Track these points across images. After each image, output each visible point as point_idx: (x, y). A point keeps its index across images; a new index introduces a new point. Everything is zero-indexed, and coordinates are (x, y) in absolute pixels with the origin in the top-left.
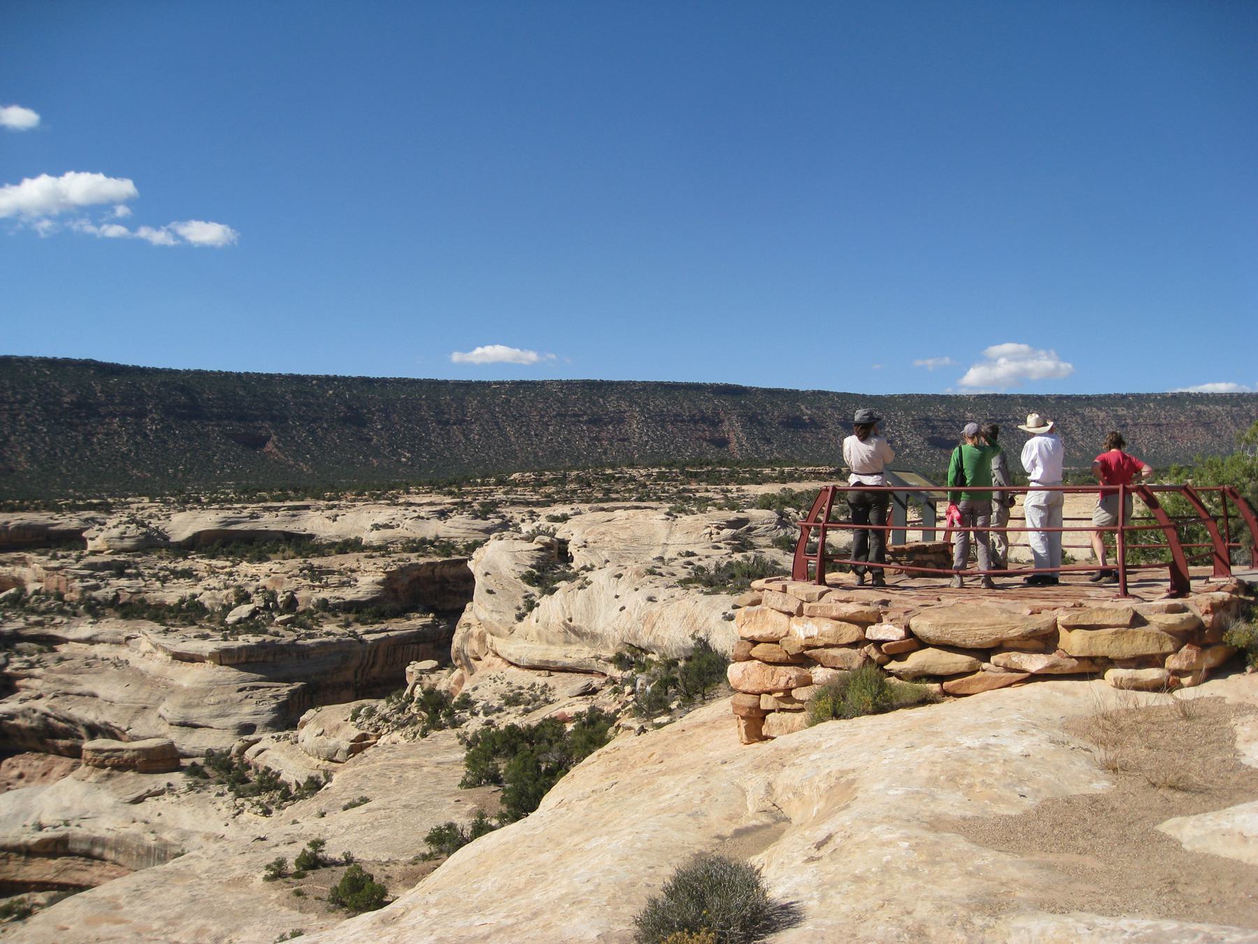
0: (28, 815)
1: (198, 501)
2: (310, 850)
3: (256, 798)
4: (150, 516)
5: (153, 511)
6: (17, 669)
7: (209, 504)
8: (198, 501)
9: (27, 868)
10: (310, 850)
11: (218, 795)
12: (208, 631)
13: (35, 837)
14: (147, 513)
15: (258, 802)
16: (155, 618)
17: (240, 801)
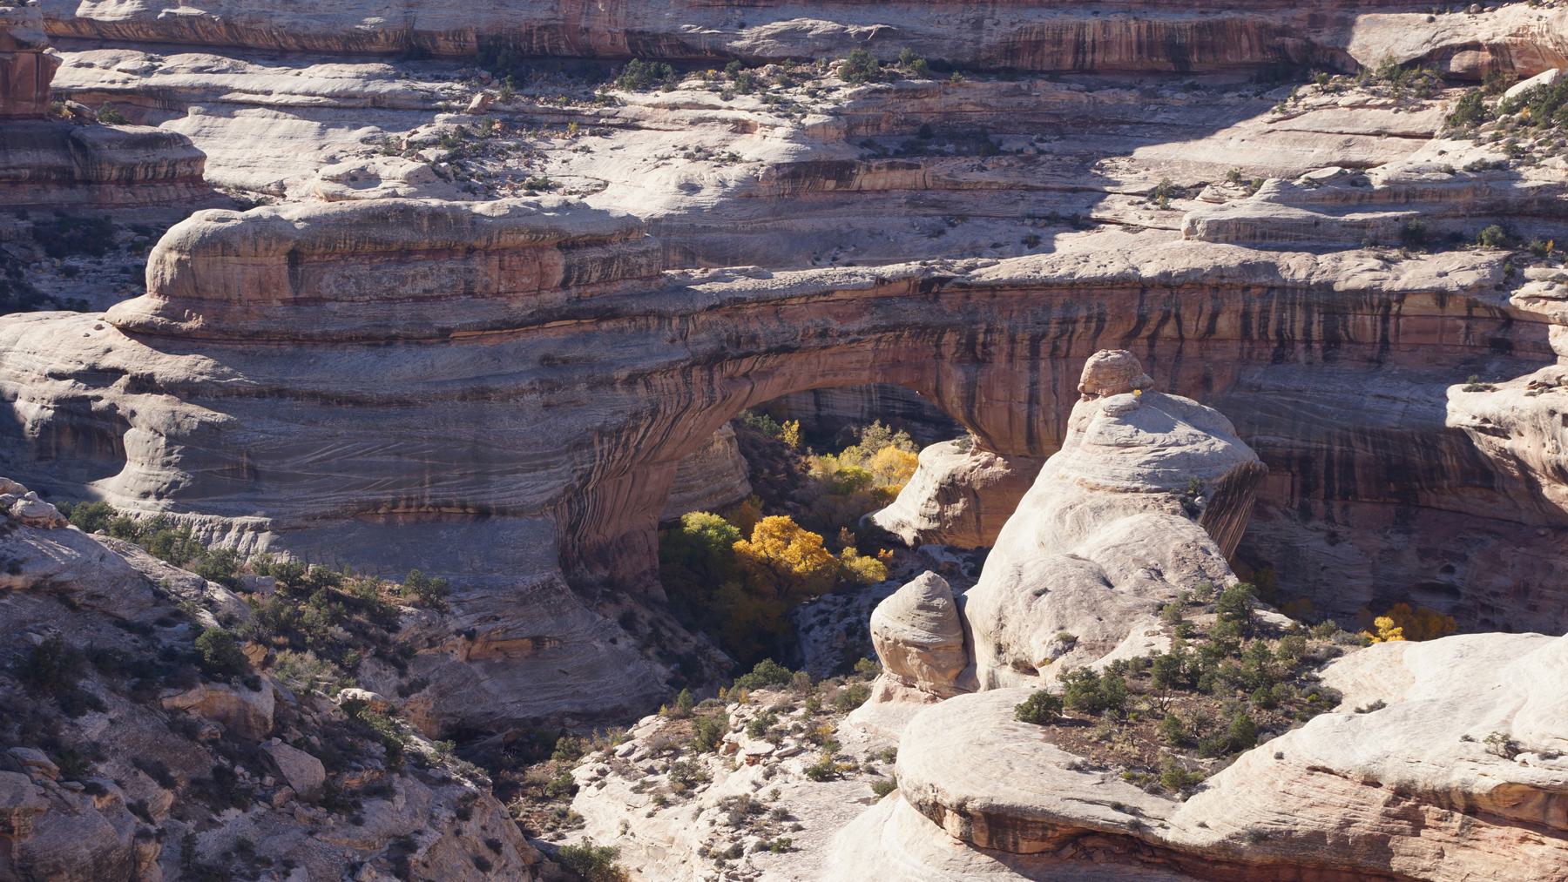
0: (1482, 711)
6: (1532, 298)
9: (1463, 855)
13: (1491, 775)
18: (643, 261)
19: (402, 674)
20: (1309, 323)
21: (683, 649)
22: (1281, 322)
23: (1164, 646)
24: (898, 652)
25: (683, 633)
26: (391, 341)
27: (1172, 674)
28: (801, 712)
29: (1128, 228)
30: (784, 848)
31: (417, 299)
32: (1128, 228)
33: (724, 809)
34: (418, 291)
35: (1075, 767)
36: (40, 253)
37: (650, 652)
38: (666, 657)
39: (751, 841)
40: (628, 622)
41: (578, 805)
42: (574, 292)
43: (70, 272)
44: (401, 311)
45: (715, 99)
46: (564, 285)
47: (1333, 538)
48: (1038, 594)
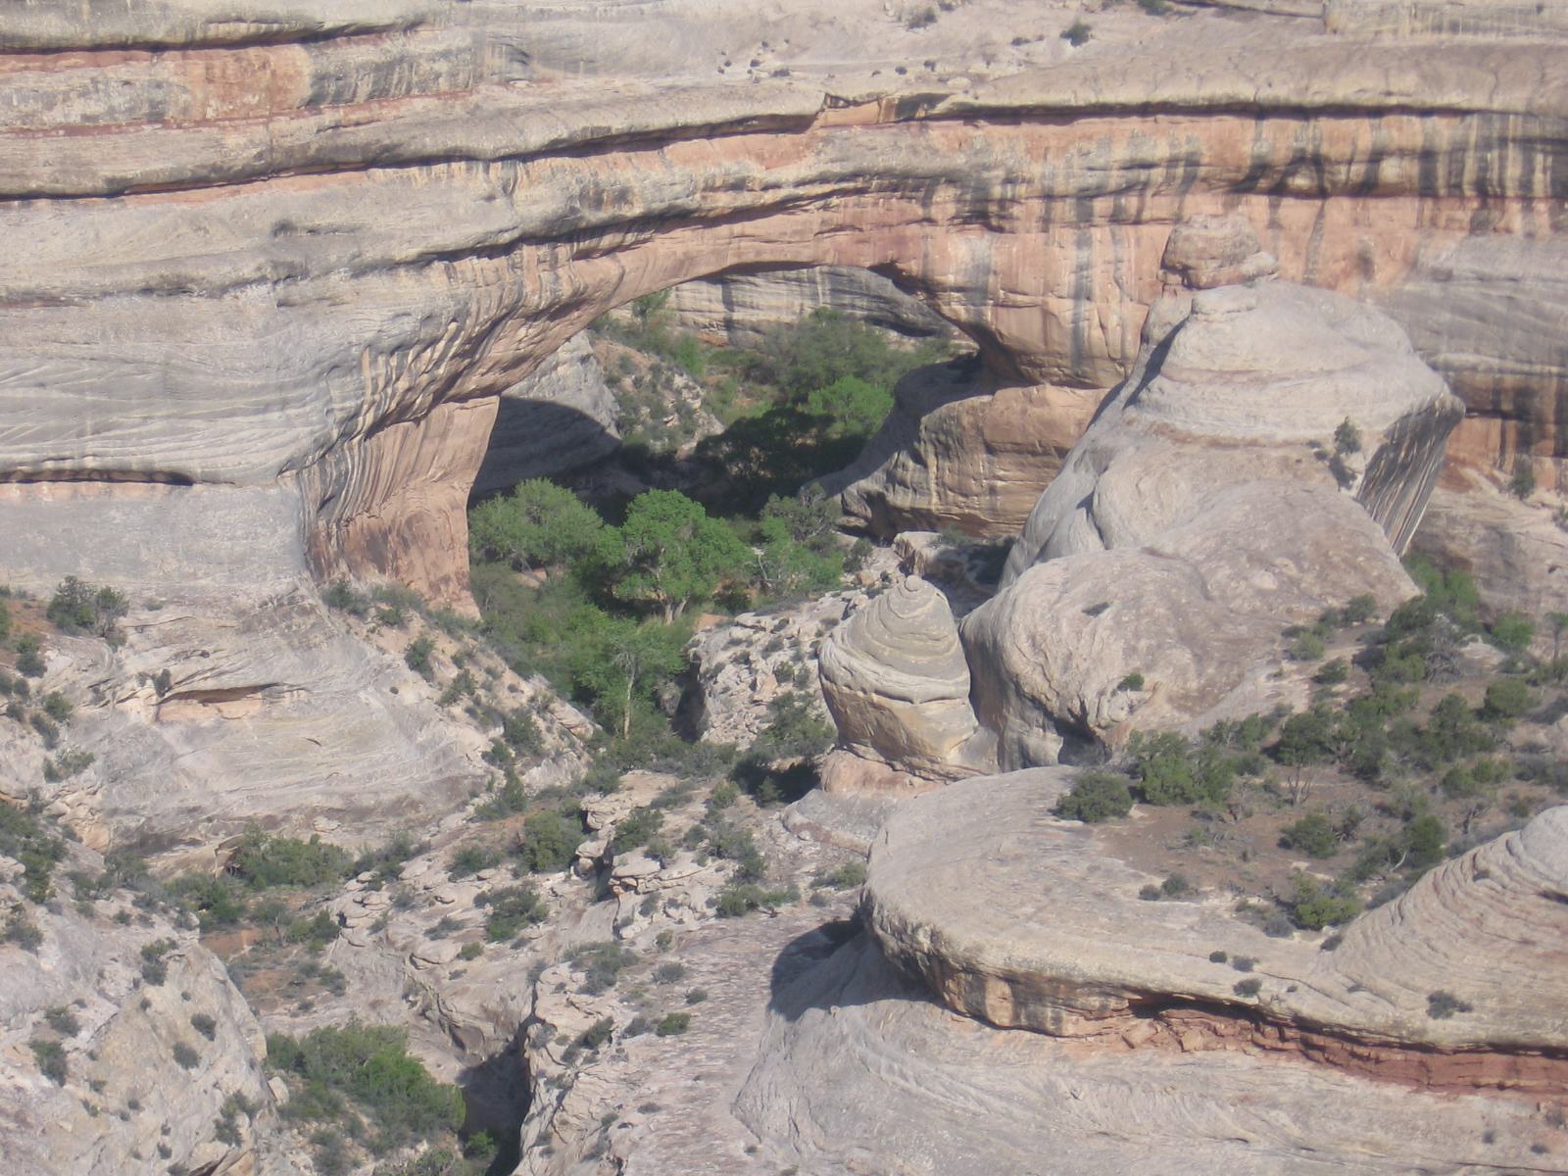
18: (442, 66)
19: (50, 745)
20: (1529, 168)
21: (509, 702)
22: (1484, 167)
23: (1299, 699)
25: (509, 677)
27: (1295, 742)
28: (699, 808)
30: (676, 1026)
31: (72, 131)
33: (575, 966)
34: (75, 118)
35: (1148, 894)
37: (457, 710)
38: (484, 715)
39: (624, 1017)
40: (419, 659)
42: (329, 117)
48: (1095, 611)
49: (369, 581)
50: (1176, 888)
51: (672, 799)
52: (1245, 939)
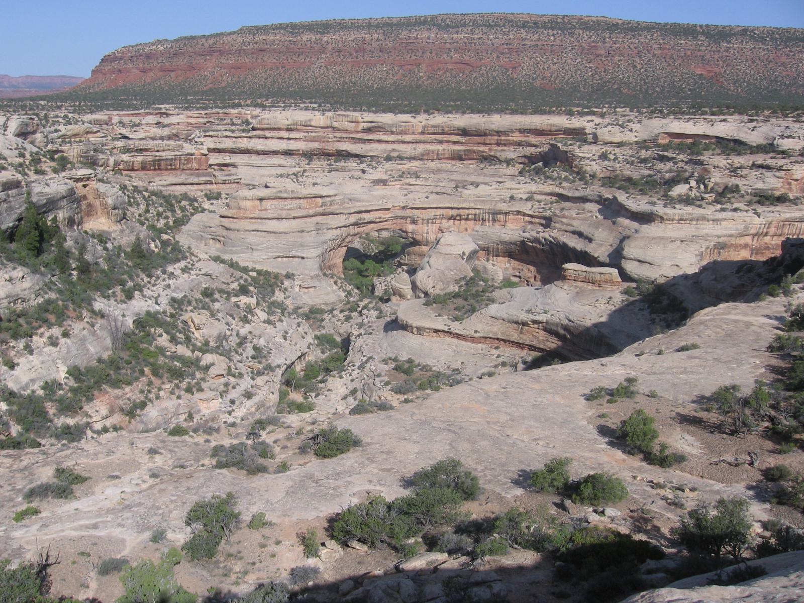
1: (661, 112)
2: (625, 384)
3: (664, 316)
4: (629, 121)
5: (632, 118)
7: (668, 114)
8: (661, 112)
10: (625, 384)
11: (640, 309)
12: (655, 200)
14: (627, 118)
15: (664, 319)
16: (745, 267)
17: (654, 316)
21: (348, 289)
24: (54, 415)
26: (282, 219)
27: (456, 295)
29: (448, 194)
30: (371, 334)
32: (448, 194)
36: (206, 199)
38: (344, 291)
41: (324, 323)
43: (212, 204)
44: (284, 212)
45: (355, 164)
46: (321, 206)
47: (493, 265)
49: (329, 272)
50: (439, 315)
51: (370, 303)
52: (449, 322)
